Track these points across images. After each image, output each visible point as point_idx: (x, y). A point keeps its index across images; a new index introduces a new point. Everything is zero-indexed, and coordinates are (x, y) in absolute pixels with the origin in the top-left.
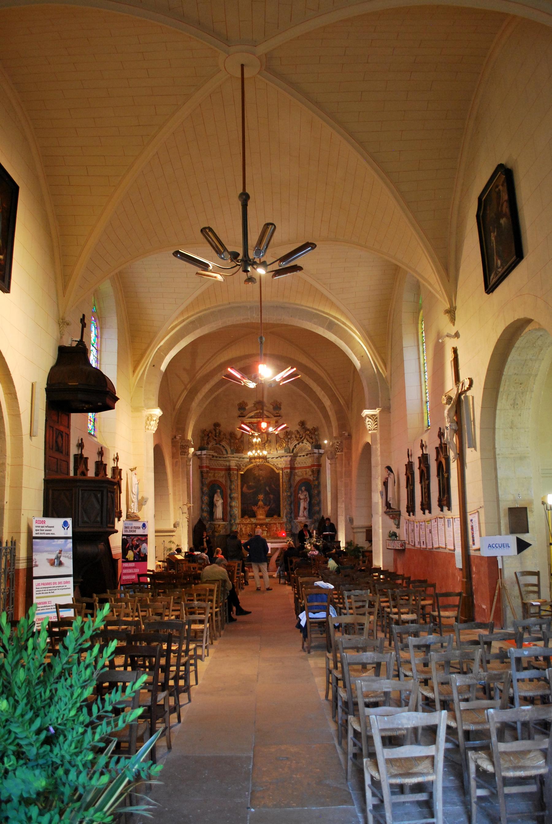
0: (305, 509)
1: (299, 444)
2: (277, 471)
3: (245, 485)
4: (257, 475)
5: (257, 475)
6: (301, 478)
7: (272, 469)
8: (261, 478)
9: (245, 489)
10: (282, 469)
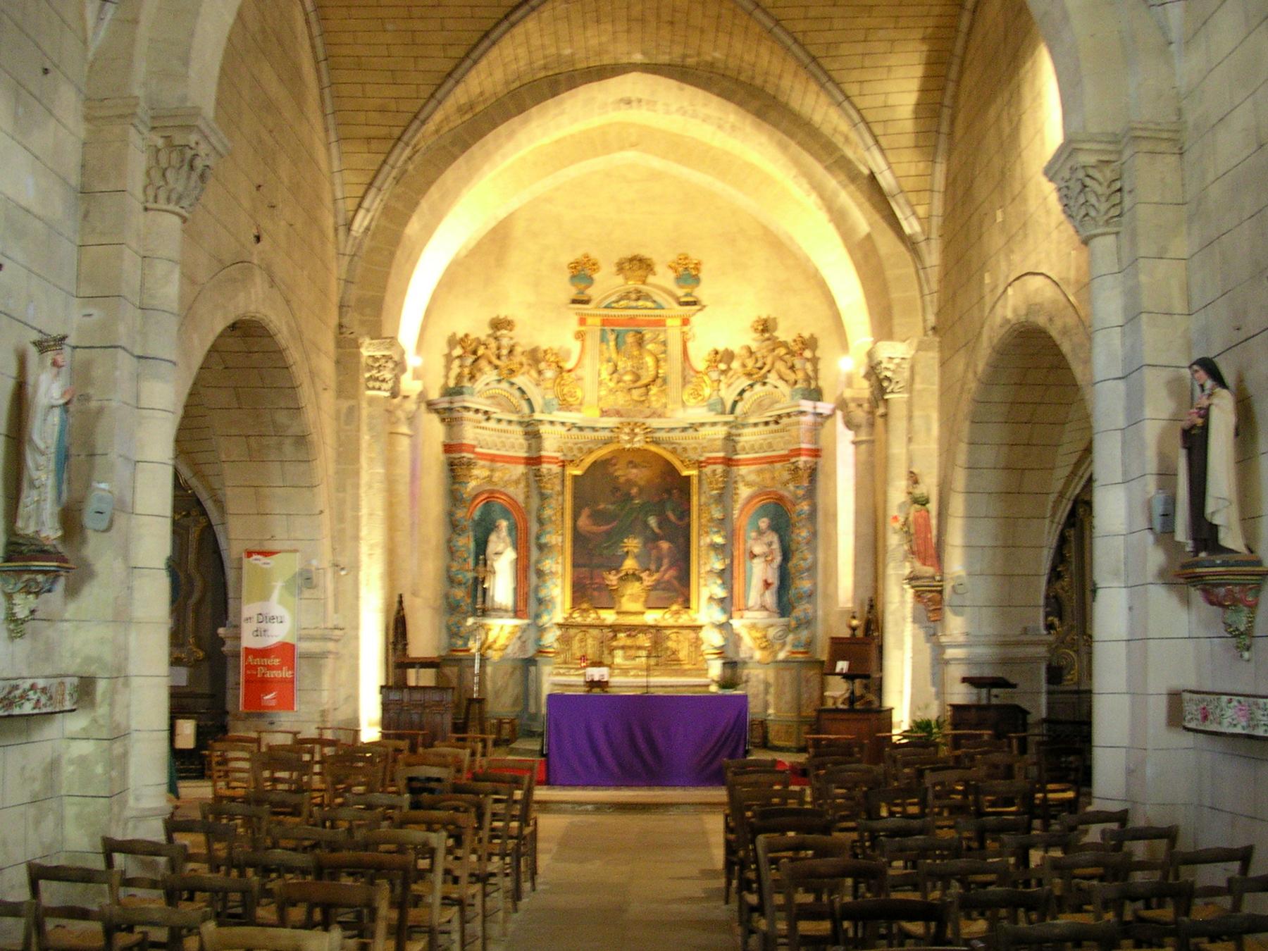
3: (586, 512)
4: (622, 480)
5: (622, 480)
7: (668, 464)
8: (634, 491)
9: (583, 521)
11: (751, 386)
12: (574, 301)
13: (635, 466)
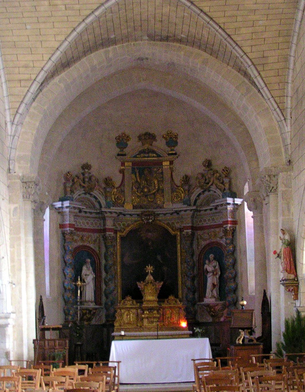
0: (214, 286)
1: (203, 192)
2: (173, 233)
6: (208, 242)
10: (181, 230)
11: (203, 192)
12: (118, 155)
13: (150, 232)
